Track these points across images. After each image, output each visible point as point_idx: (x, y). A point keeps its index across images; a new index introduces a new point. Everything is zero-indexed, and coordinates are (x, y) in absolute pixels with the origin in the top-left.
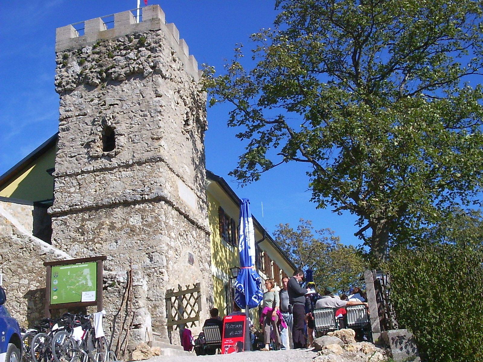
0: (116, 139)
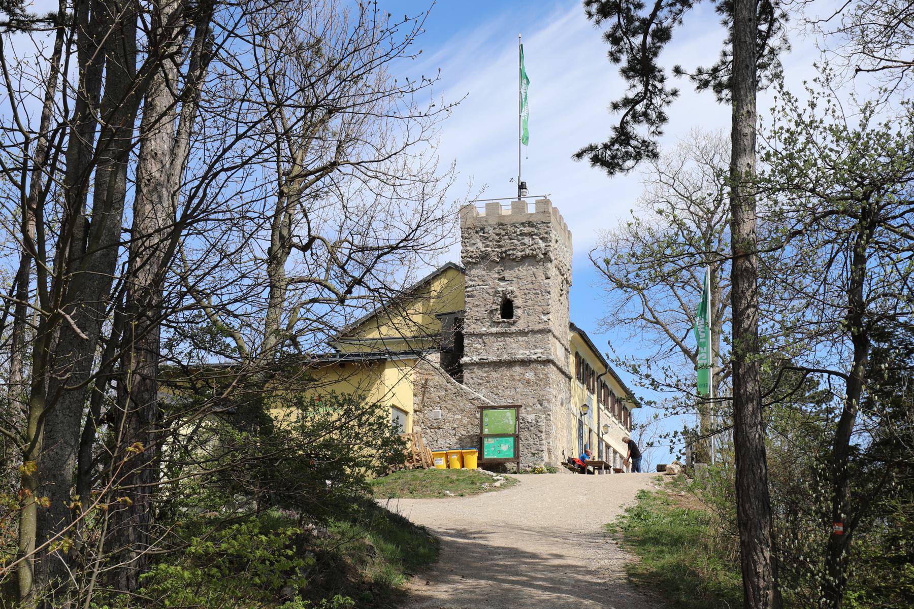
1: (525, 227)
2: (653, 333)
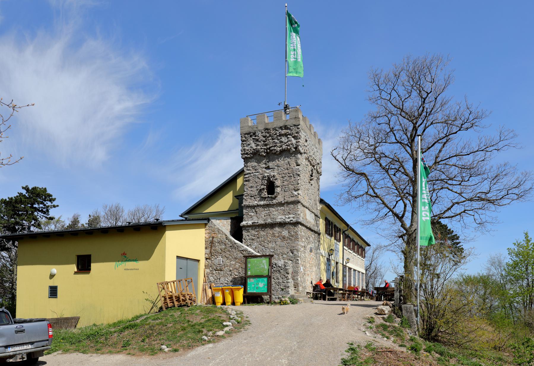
2: (374, 204)
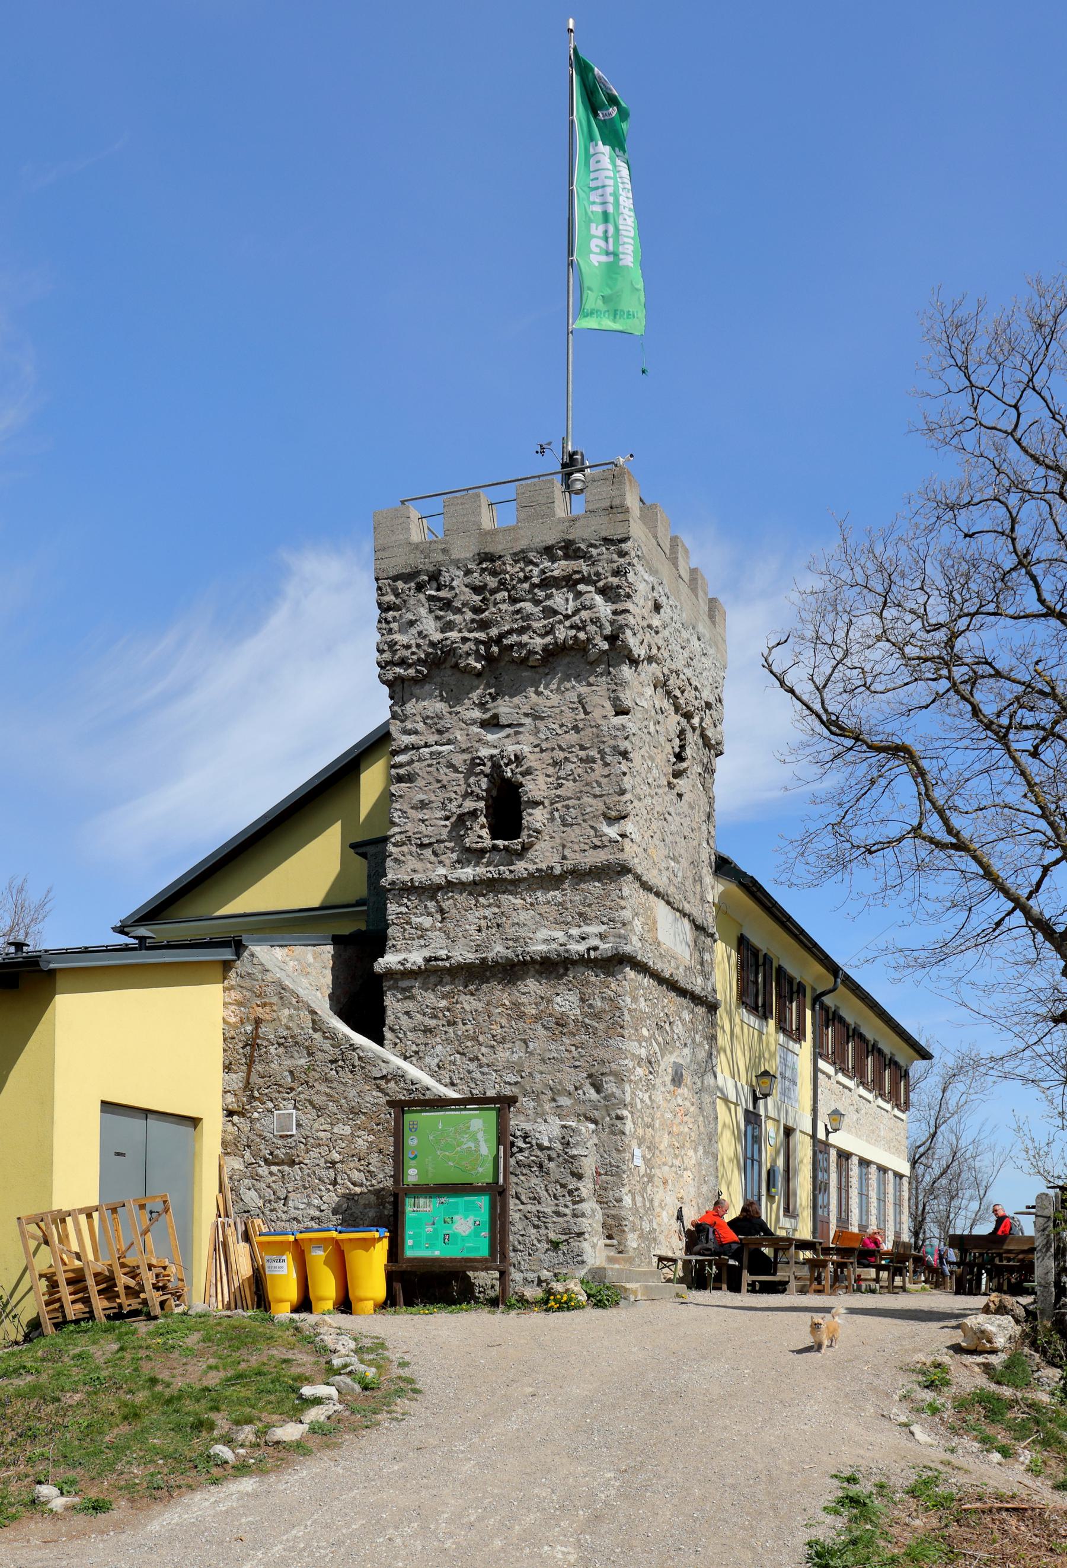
0: (525, 813)
1: (553, 559)
